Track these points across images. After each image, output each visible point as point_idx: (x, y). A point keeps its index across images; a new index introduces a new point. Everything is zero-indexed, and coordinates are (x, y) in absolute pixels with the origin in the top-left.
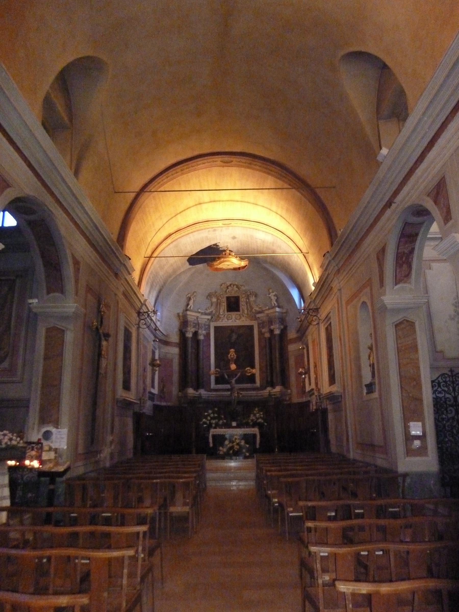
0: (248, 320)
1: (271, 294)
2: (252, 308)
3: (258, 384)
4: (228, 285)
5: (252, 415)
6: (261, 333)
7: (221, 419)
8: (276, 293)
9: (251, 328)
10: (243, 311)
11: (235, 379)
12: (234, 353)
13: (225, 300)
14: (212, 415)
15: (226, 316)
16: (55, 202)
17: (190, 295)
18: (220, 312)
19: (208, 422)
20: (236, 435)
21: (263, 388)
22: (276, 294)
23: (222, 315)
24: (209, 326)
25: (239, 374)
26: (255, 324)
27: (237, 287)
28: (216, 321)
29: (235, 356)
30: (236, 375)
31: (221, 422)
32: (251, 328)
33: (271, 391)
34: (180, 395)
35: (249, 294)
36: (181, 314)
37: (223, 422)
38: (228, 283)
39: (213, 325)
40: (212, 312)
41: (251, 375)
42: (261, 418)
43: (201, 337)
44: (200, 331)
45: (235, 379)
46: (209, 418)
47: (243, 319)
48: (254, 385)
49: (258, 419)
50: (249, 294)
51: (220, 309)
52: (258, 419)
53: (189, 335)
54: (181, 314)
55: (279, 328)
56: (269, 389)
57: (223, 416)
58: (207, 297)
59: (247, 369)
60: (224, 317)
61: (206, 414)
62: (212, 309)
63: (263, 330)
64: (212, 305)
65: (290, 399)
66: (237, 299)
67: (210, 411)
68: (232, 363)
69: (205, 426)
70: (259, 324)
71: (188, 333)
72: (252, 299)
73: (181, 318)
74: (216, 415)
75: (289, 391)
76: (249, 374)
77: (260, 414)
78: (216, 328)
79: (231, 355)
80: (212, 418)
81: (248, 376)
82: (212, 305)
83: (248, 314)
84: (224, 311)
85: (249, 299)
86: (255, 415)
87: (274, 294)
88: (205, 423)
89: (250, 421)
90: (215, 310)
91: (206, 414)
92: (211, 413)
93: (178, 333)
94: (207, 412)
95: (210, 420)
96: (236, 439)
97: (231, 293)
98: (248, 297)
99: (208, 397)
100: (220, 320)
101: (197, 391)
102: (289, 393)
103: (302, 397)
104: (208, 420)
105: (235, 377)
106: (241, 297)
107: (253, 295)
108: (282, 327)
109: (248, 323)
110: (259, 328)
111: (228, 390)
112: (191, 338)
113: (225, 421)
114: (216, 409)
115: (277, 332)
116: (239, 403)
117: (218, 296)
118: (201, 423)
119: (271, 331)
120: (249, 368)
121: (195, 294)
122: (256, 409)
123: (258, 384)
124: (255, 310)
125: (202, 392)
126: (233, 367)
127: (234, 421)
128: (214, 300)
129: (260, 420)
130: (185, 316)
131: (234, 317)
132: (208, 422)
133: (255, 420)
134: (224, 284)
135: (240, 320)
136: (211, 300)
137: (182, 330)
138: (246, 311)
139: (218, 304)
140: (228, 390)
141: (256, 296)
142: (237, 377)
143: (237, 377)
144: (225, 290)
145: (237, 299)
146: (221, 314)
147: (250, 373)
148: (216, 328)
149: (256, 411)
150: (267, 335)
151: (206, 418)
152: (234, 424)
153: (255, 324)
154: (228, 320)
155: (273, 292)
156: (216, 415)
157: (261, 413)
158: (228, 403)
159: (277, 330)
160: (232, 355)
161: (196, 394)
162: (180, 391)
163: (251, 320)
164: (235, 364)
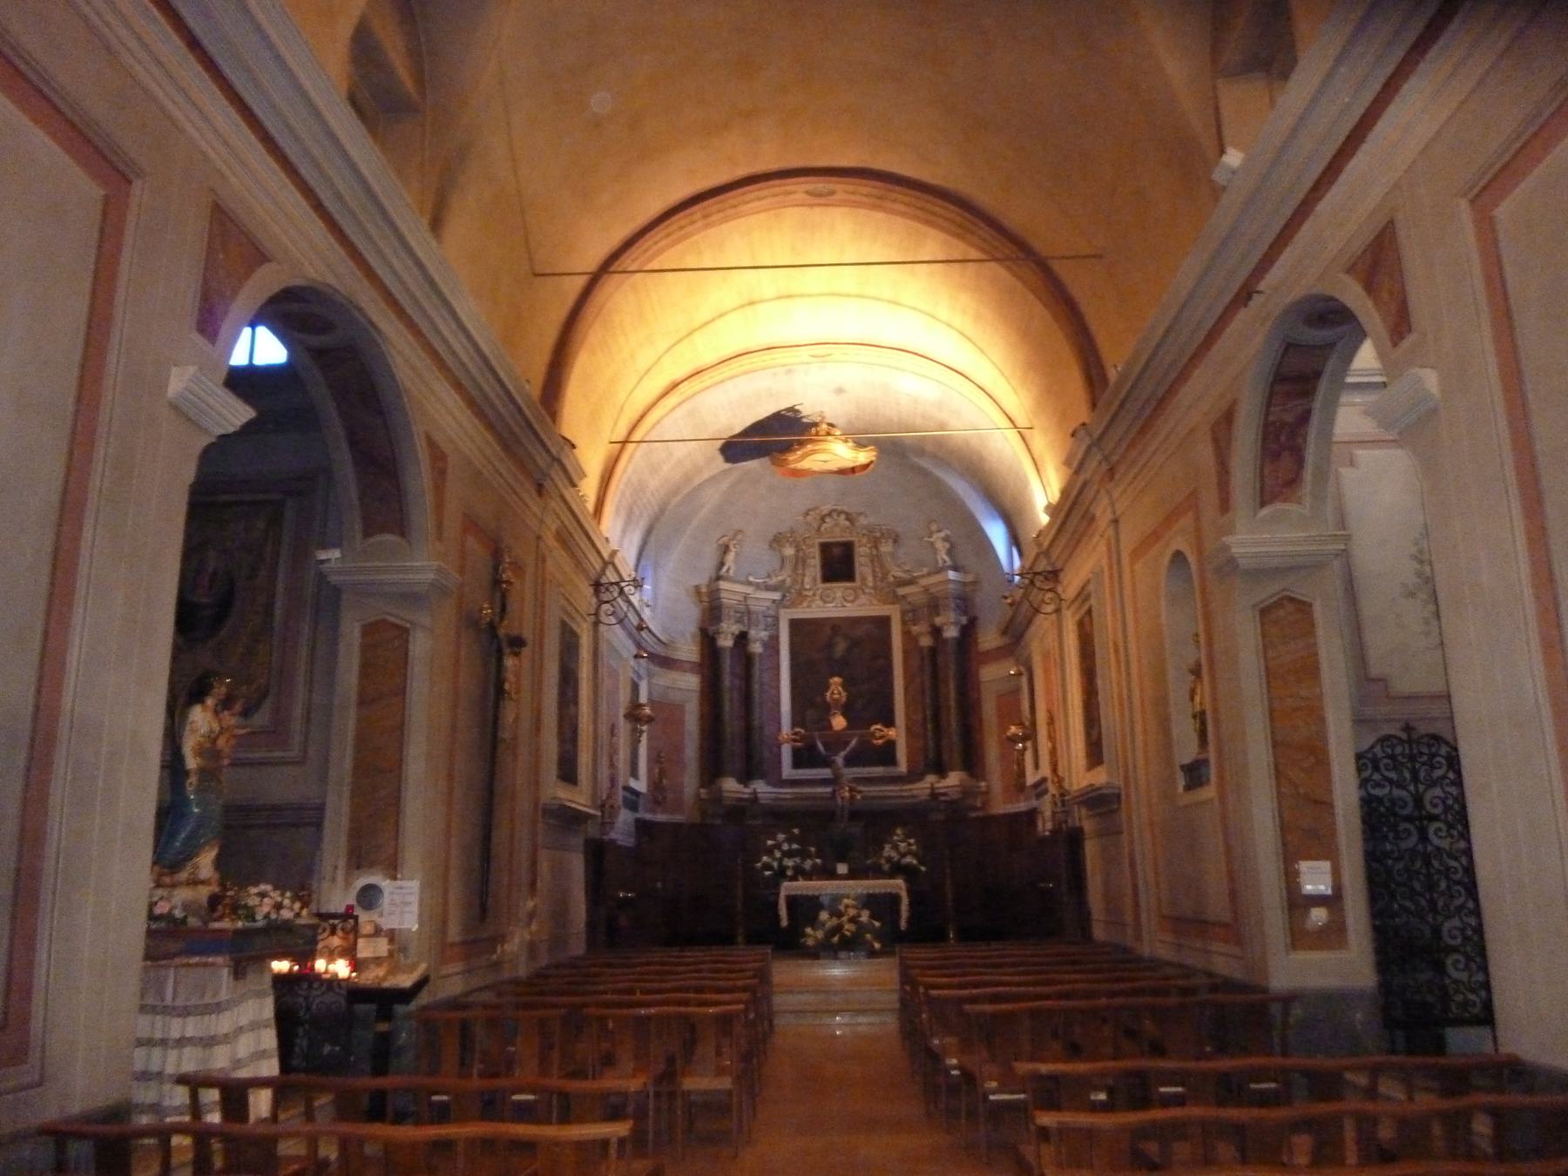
0: (875, 602)
2: (886, 574)
5: (887, 847)
8: (948, 532)
9: (883, 622)
11: (843, 754)
12: (840, 689)
13: (816, 552)
14: (785, 847)
18: (803, 582)
19: (775, 864)
21: (914, 776)
23: (810, 589)
24: (776, 619)
26: (894, 612)
27: (849, 517)
28: (793, 605)
30: (847, 743)
33: (937, 785)
34: (703, 796)
35: (878, 534)
42: (910, 853)
43: (756, 648)
44: (753, 633)
45: (843, 754)
46: (778, 854)
47: (863, 599)
52: (903, 855)
53: (726, 642)
54: (704, 590)
56: (931, 779)
57: (813, 849)
58: (771, 546)
60: (814, 595)
61: (770, 842)
63: (916, 629)
65: (986, 804)
66: (848, 548)
67: (781, 837)
69: (767, 873)
70: (904, 613)
71: (722, 636)
72: (886, 548)
73: (705, 599)
74: (795, 846)
75: (983, 784)
77: (910, 844)
78: (795, 625)
79: (833, 693)
85: (876, 547)
86: (895, 847)
87: (942, 534)
88: (767, 867)
91: (770, 842)
92: (784, 841)
98: (875, 543)
100: (805, 604)
101: (746, 786)
102: (984, 789)
104: (774, 859)
106: (857, 545)
108: (964, 620)
110: (904, 623)
114: (796, 831)
115: (951, 633)
118: (759, 865)
119: (936, 631)
120: (878, 727)
122: (899, 831)
123: (903, 767)
125: (761, 787)
127: (842, 861)
129: (908, 859)
131: (839, 594)
132: (775, 864)
138: (870, 578)
139: (800, 561)
147: (881, 737)
148: (795, 625)
150: (926, 641)
151: (770, 852)
152: (842, 869)
153: (894, 612)
154: (825, 602)
157: (912, 841)
159: (953, 628)
161: (744, 793)
162: (702, 786)
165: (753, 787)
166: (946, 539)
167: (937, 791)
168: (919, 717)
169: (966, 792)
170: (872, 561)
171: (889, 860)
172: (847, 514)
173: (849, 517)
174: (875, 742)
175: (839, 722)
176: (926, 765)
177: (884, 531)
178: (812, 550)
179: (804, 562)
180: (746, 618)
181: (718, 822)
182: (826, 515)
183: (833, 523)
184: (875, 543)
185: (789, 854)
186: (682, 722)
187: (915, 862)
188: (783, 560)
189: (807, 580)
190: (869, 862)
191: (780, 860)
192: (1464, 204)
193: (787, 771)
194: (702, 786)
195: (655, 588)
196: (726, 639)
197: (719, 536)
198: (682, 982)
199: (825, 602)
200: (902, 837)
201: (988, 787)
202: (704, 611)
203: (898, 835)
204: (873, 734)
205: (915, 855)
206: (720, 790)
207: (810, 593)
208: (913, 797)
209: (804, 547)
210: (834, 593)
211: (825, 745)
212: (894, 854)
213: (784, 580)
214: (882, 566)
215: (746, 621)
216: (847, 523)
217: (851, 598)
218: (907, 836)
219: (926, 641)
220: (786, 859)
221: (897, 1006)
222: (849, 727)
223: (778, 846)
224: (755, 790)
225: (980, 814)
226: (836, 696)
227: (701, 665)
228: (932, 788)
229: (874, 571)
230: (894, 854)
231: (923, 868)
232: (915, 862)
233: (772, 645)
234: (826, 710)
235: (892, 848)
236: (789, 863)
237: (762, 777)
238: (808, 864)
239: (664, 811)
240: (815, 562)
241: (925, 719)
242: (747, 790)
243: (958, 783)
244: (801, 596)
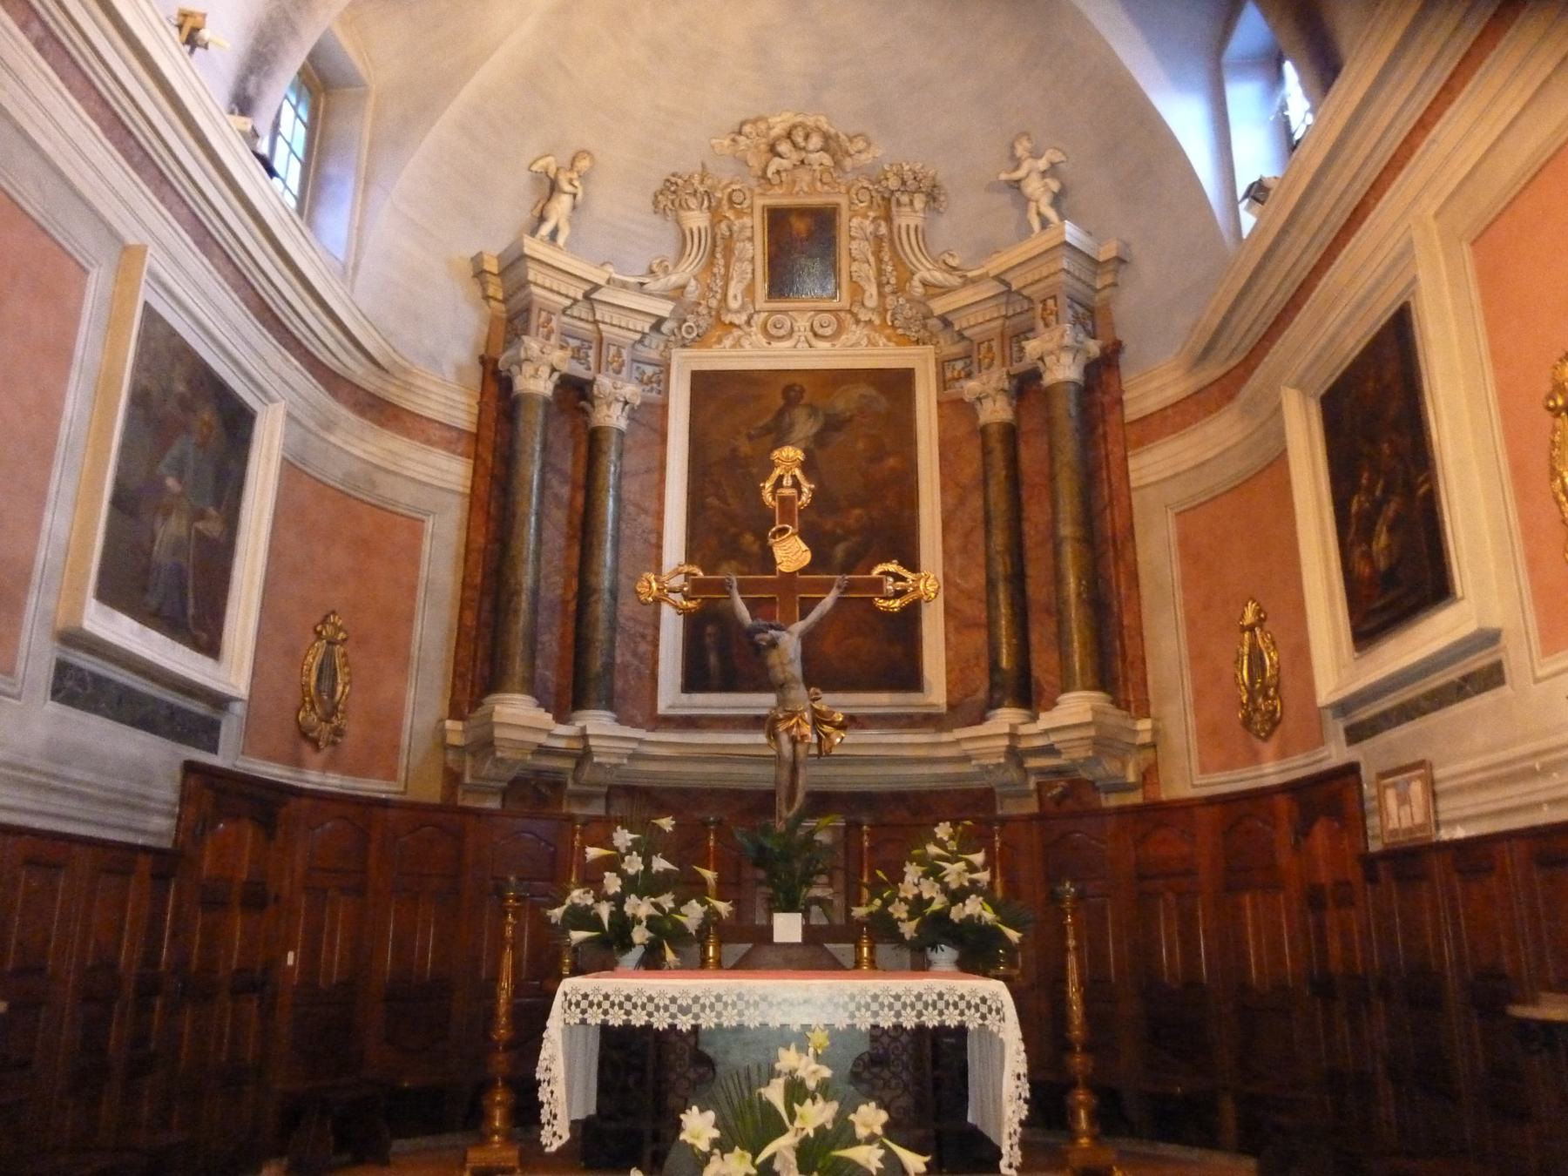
0: (882, 341)
1: (1025, 167)
2: (906, 274)
3: (936, 690)
4: (777, 131)
5: (912, 872)
6: (955, 408)
7: (696, 889)
8: (1057, 157)
9: (898, 383)
10: (857, 290)
11: (799, 626)
12: (797, 472)
13: (756, 224)
14: (634, 865)
15: (758, 319)
16: (976, 1126)
17: (550, 163)
18: (725, 295)
19: (604, 910)
20: (801, 1040)
21: (966, 710)
22: (1053, 165)
23: (738, 312)
24: (664, 367)
25: (829, 600)
26: (922, 361)
27: (830, 143)
28: (701, 340)
29: (807, 487)
30: (807, 607)
31: (693, 914)
32: (898, 383)
33: (1024, 730)
34: (455, 739)
35: (893, 183)
36: (492, 266)
37: (712, 914)
38: (779, 124)
39: (684, 364)
40: (682, 288)
41: (903, 609)
42: (974, 888)
43: (612, 417)
44: (604, 383)
45: (799, 626)
46: (613, 883)
47: (855, 333)
48: (913, 697)
49: (958, 896)
50: (893, 183)
51: (727, 279)
52: (958, 896)
53: (536, 383)
54: (492, 266)
55: (1076, 351)
56: (1006, 718)
57: (709, 875)
58: (656, 203)
59: (876, 572)
60: (748, 323)
61: (593, 852)
62: (685, 273)
63: (971, 387)
64: (681, 253)
65: (1149, 775)
66: (824, 221)
67: (623, 838)
68: (783, 531)
69: (577, 936)
70: (942, 364)
71: (528, 369)
72: (909, 218)
73: (495, 289)
74: (660, 864)
75: (1144, 725)
76: (896, 604)
77: (972, 868)
78: (705, 385)
79: (779, 483)
80: (632, 885)
81: (887, 615)
82: (681, 253)
83: (882, 310)
84: (750, 290)
85: (888, 219)
86: (933, 871)
87: (1042, 164)
88: (582, 918)
89: (899, 911)
90: (696, 278)
91: (593, 852)
92: (629, 851)
93: (475, 376)
94: (606, 842)
95: (619, 900)
96: (796, 1091)
97: (794, 182)
98: (886, 207)
99: (634, 757)
100: (728, 342)
101: (561, 718)
102: (1146, 738)
103: (1255, 758)
104: (600, 897)
105: (803, 616)
106: (844, 214)
107: (919, 190)
108: (1094, 347)
109: (886, 355)
110: (944, 383)
111: (755, 723)
112: (547, 403)
113: (723, 907)
114: (667, 823)
115: (1064, 371)
116: (821, 802)
117: (720, 201)
118: (557, 914)
119: (1026, 385)
120: (892, 567)
121: (583, 164)
122: (943, 831)
123: (936, 690)
124: (925, 284)
125: (597, 723)
126: (791, 553)
127: (790, 908)
128: (697, 219)
129: (973, 907)
130: (515, 262)
131: (802, 323)
132: (604, 910)
133: (936, 906)
134: (755, 122)
135: (838, 344)
136: (678, 222)
137: (496, 361)
138: (872, 290)
139: (720, 247)
140: (755, 723)
141: (933, 196)
142: (814, 616)
143: (814, 616)
144: (755, 163)
145: (824, 221)
146: (734, 304)
147: (898, 594)
148: (705, 385)
149: (941, 844)
150: (996, 411)
151: (591, 879)
152: (787, 928)
153: (922, 361)
154: (771, 338)
155: (1036, 155)
156: (660, 864)
157: (978, 858)
158: (760, 803)
159: (1066, 358)
160: (787, 481)
161: (551, 735)
162: (455, 712)
163: (904, 340)
164: (804, 535)
165: (579, 724)
166: (1052, 171)
167: (1024, 744)
168: (978, 579)
169: (1104, 743)
170: (877, 253)
171: (918, 904)
172: (826, 137)
173: (830, 143)
174: (881, 603)
175: (791, 553)
176: (993, 687)
177: (908, 176)
178: (747, 221)
179: (728, 252)
180: (592, 353)
181: (493, 804)
182: (778, 139)
183: (795, 157)
184: (886, 207)
185: (647, 885)
186: (412, 553)
187: (989, 916)
188: (683, 240)
189: (735, 288)
190: (859, 912)
191: (619, 900)
192: (1466, 248)
193: (670, 695)
194: (455, 712)
195: (359, 232)
196: (535, 375)
197: (537, 154)
198: (1517, 555)
199: (771, 338)
200: (952, 846)
201: (1155, 731)
202: (493, 321)
203: (941, 844)
204: (877, 585)
205: (987, 894)
206: (489, 724)
207: (740, 319)
208: (966, 759)
209: (730, 214)
210: (793, 319)
211: (752, 605)
212: (929, 890)
213: (683, 287)
214: (898, 261)
215: (592, 359)
216: (826, 159)
217: (828, 332)
218: (967, 843)
219: (996, 411)
220: (632, 899)
221: (468, 491)
222: (820, 561)
223: (613, 864)
224: (584, 729)
225: (1136, 798)
226: (788, 492)
227: (476, 438)
228: (1013, 736)
229: (880, 272)
230: (929, 890)
231: (1013, 935)
232: (989, 916)
233: (651, 417)
234: (762, 524)
235: (926, 875)
236: (641, 908)
237: (610, 706)
238: (693, 914)
239: (330, 765)
240: (753, 250)
241: (991, 584)
242: (561, 729)
243: (1088, 718)
244: (721, 325)
